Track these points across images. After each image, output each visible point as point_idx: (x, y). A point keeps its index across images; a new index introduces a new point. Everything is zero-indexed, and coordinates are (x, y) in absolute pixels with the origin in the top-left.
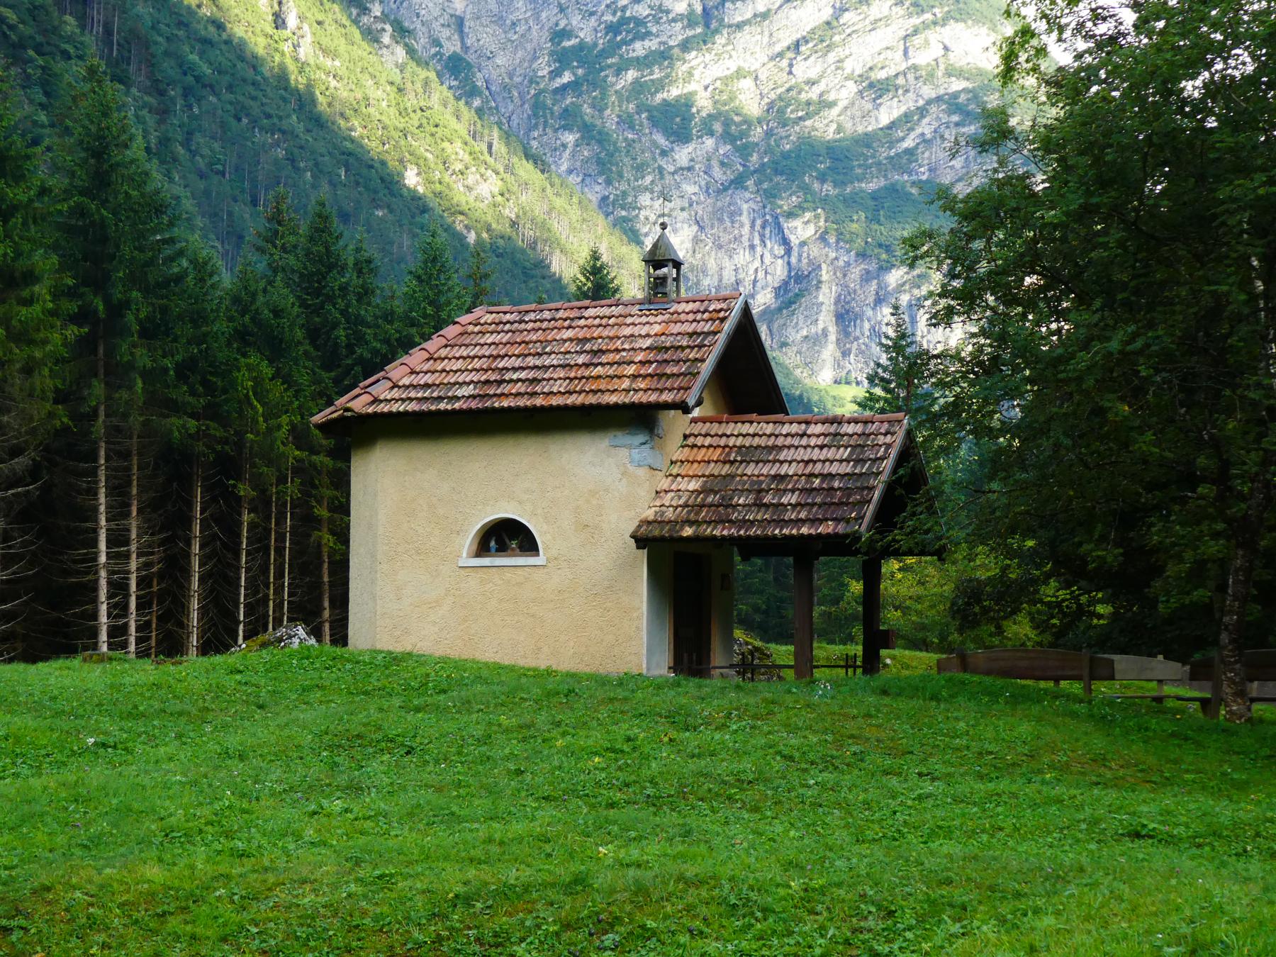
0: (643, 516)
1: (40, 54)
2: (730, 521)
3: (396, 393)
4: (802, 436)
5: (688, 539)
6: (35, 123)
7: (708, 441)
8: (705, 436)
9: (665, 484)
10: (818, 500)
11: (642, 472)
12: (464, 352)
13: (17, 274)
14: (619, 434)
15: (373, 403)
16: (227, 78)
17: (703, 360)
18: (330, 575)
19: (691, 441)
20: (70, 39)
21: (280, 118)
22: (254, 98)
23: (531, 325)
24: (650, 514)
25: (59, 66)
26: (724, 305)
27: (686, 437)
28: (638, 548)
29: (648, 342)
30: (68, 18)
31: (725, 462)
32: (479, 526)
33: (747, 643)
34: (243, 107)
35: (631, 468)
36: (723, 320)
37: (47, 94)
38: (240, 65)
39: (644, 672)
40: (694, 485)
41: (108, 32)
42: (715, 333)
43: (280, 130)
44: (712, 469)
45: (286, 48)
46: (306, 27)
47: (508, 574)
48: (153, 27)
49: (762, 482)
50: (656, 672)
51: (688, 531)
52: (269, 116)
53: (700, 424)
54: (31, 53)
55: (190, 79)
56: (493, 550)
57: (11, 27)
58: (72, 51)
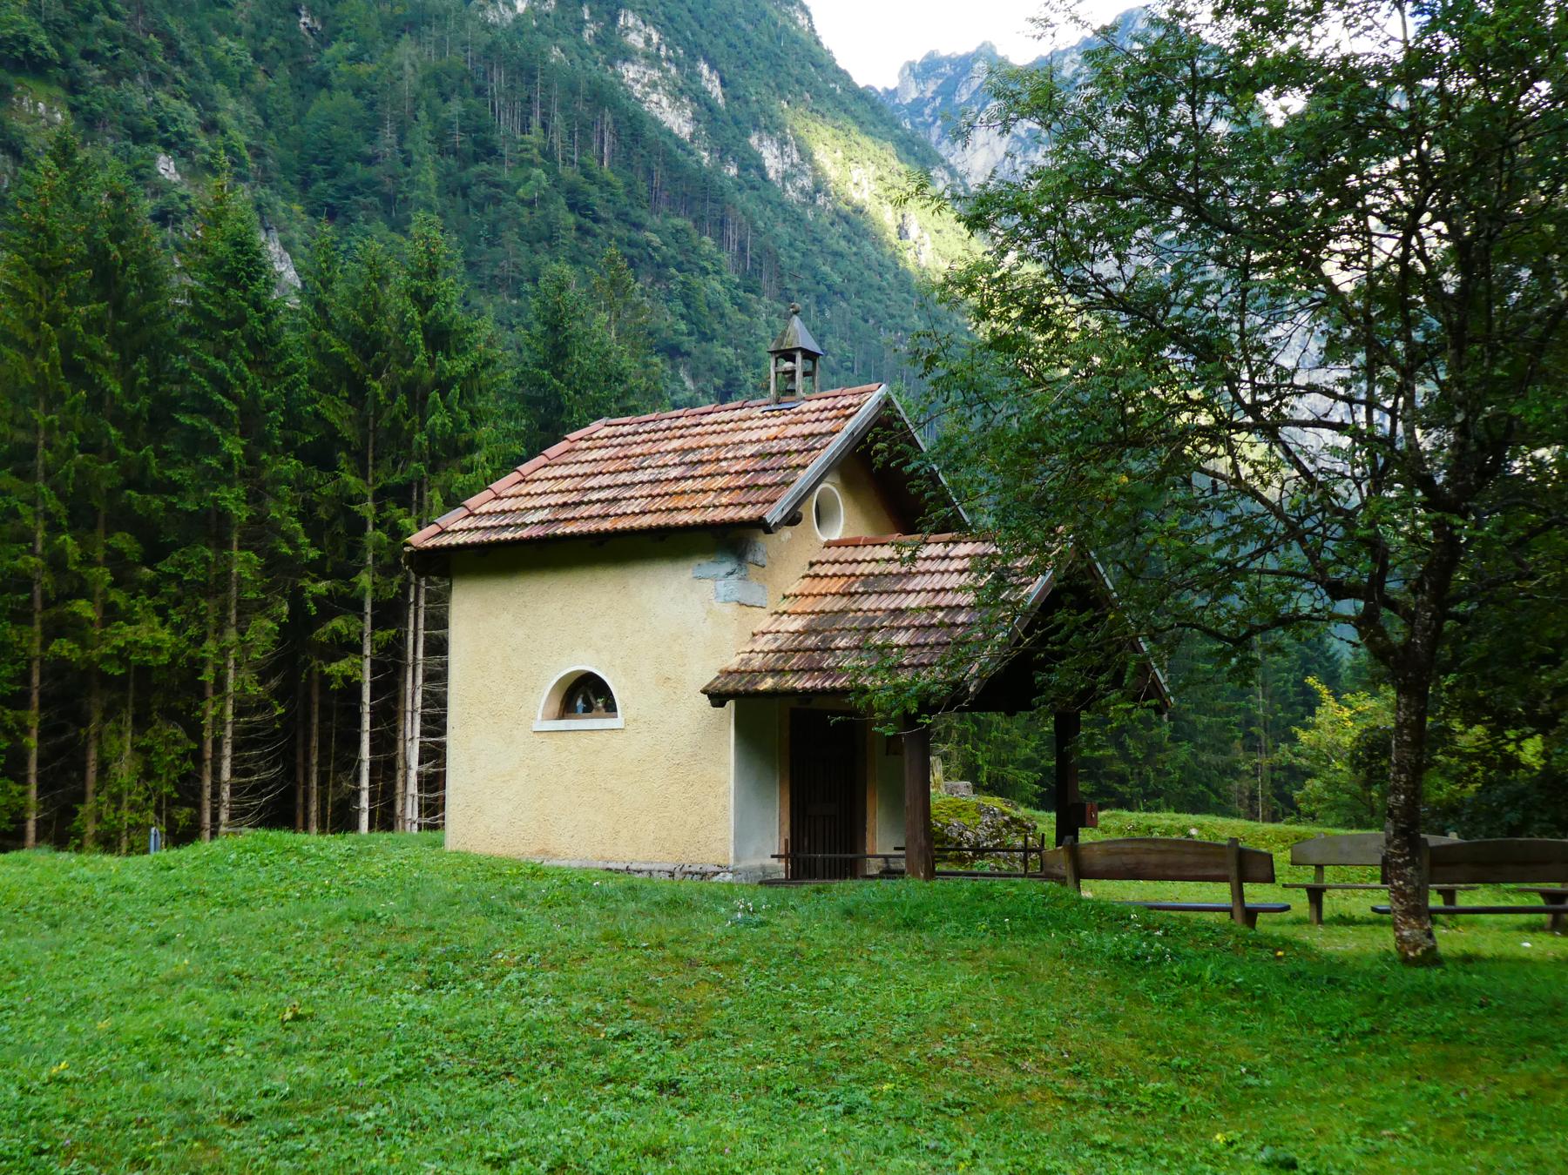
0: (724, 666)
1: (680, 270)
2: (820, 669)
3: (470, 522)
4: (944, 558)
5: (765, 693)
6: (675, 331)
7: (836, 568)
8: (834, 563)
9: (765, 623)
10: (932, 640)
11: (730, 610)
12: (573, 470)
13: (460, 444)
14: (703, 562)
15: (439, 534)
16: (856, 284)
17: (805, 467)
18: (373, 750)
19: (817, 569)
20: (708, 258)
21: (903, 318)
22: (879, 302)
23: (645, 436)
24: (733, 663)
25: (697, 281)
26: (856, 401)
27: (812, 565)
28: (714, 705)
29: (749, 450)
30: (706, 238)
31: (843, 595)
32: (554, 681)
33: (1003, 814)
34: (870, 310)
35: (717, 605)
36: (848, 417)
37: (687, 306)
38: (866, 273)
39: (731, 862)
40: (797, 624)
41: (742, 249)
42: (833, 433)
43: (903, 329)
44: (829, 604)
45: (909, 255)
46: (926, 235)
47: (585, 740)
48: (791, 245)
49: (875, 618)
50: (755, 862)
51: (767, 684)
52: (892, 316)
53: (834, 549)
54: (673, 270)
55: (822, 288)
56: (580, 710)
57: (656, 249)
58: (710, 267)
